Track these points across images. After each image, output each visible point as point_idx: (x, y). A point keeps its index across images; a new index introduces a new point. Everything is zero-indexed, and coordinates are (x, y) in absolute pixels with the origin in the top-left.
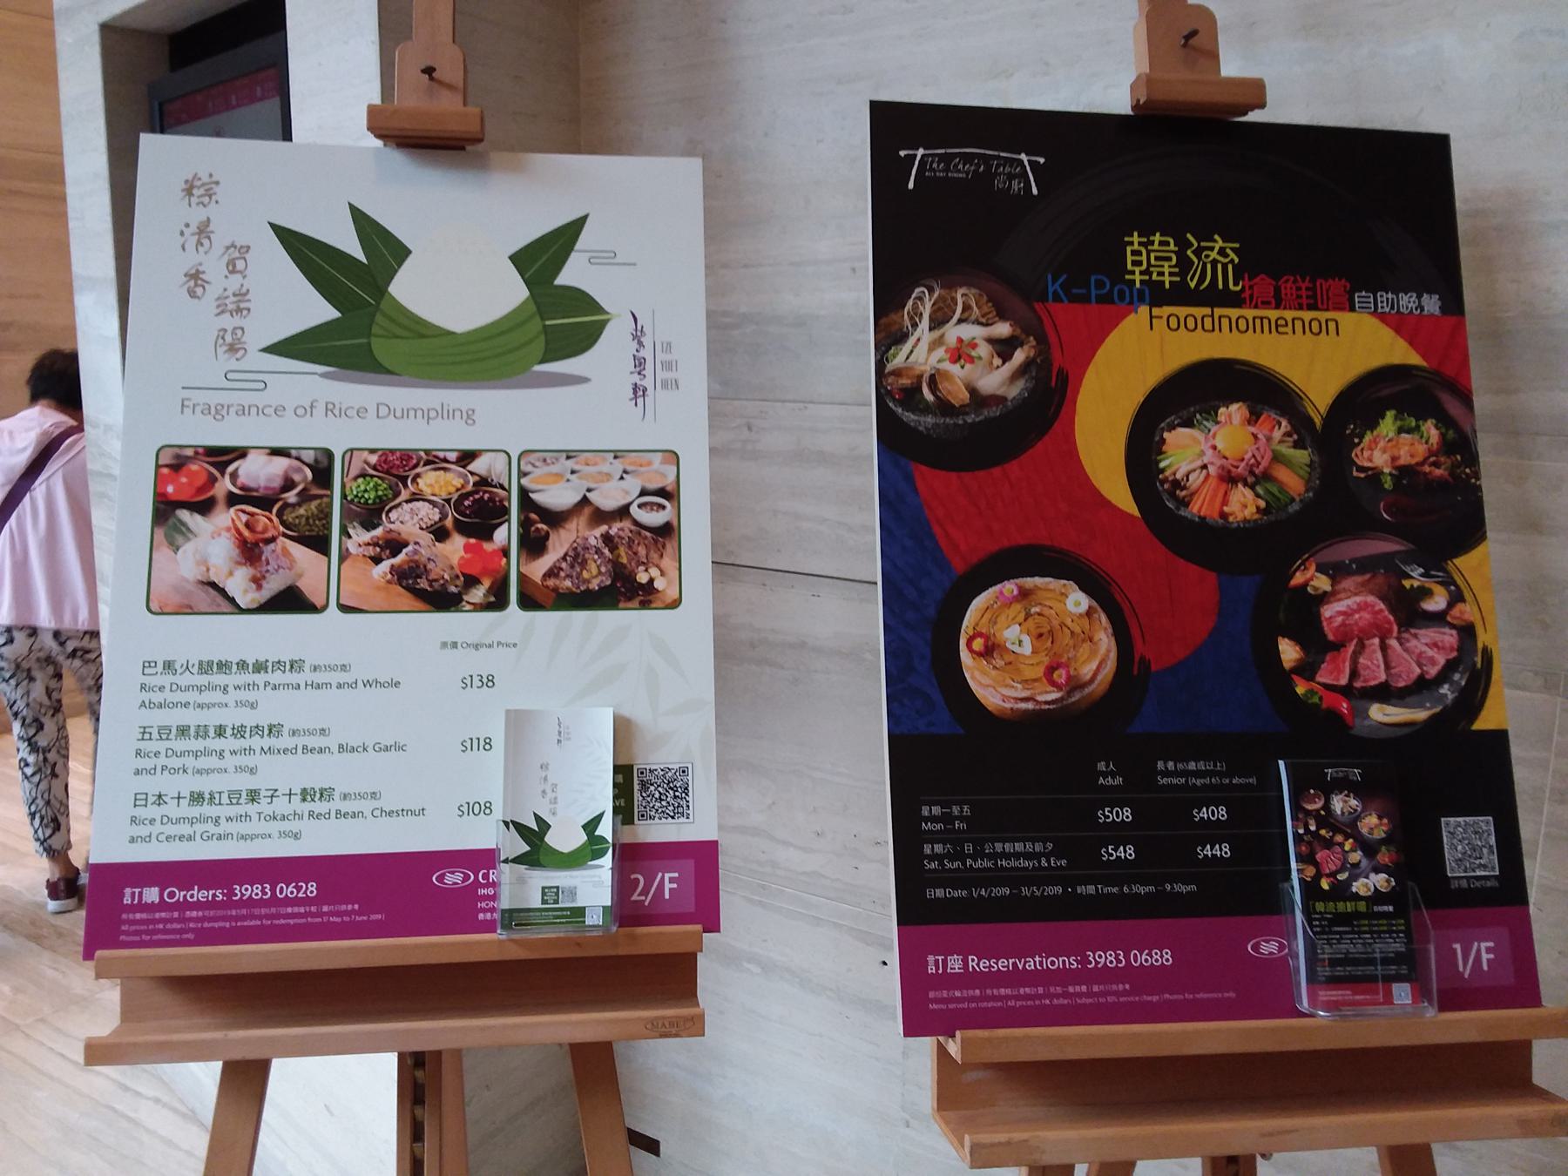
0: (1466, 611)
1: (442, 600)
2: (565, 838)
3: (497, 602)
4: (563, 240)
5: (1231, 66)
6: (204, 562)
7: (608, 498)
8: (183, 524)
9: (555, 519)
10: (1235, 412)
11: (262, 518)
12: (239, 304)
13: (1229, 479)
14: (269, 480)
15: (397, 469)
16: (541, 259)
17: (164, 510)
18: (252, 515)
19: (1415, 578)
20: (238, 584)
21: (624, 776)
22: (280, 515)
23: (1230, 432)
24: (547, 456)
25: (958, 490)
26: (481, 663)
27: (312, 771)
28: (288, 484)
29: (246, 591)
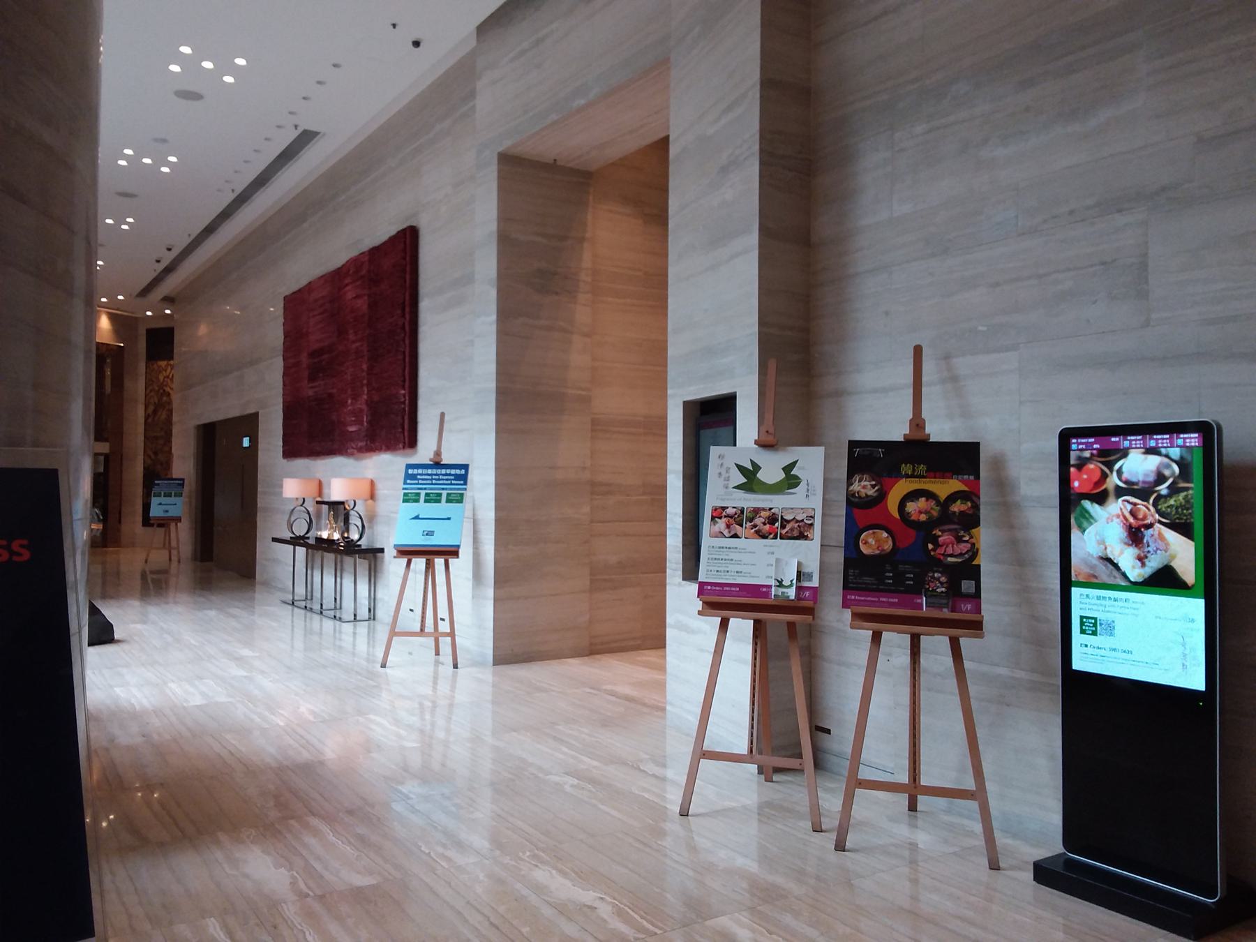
0: (973, 540)
1: (764, 537)
2: (786, 583)
3: (775, 538)
4: (793, 464)
5: (927, 431)
6: (1102, 542)
7: (799, 518)
8: (1087, 512)
9: (788, 522)
10: (923, 499)
11: (1142, 506)
12: (728, 479)
13: (920, 512)
14: (1146, 475)
15: (756, 511)
16: (788, 469)
17: (713, 518)
18: (1135, 504)
19: (962, 533)
20: (726, 532)
21: (799, 573)
22: (1155, 505)
23: (922, 503)
24: (787, 509)
25: (861, 513)
26: (772, 549)
27: (739, 568)
28: (1161, 478)
29: (1134, 567)
